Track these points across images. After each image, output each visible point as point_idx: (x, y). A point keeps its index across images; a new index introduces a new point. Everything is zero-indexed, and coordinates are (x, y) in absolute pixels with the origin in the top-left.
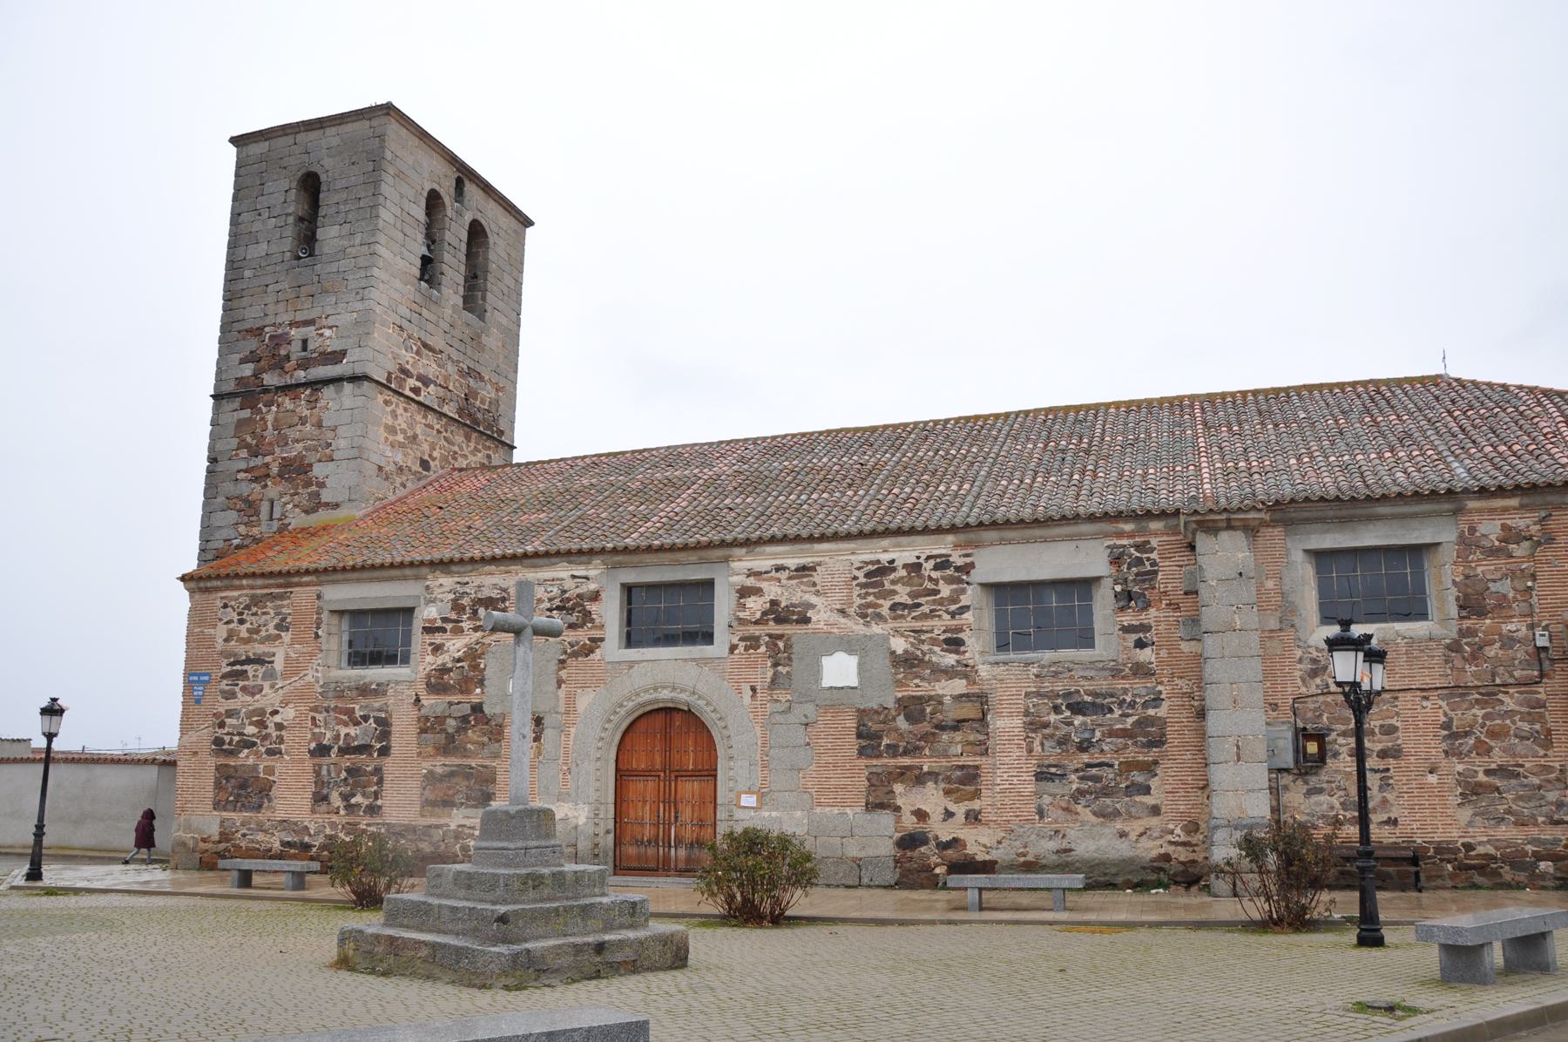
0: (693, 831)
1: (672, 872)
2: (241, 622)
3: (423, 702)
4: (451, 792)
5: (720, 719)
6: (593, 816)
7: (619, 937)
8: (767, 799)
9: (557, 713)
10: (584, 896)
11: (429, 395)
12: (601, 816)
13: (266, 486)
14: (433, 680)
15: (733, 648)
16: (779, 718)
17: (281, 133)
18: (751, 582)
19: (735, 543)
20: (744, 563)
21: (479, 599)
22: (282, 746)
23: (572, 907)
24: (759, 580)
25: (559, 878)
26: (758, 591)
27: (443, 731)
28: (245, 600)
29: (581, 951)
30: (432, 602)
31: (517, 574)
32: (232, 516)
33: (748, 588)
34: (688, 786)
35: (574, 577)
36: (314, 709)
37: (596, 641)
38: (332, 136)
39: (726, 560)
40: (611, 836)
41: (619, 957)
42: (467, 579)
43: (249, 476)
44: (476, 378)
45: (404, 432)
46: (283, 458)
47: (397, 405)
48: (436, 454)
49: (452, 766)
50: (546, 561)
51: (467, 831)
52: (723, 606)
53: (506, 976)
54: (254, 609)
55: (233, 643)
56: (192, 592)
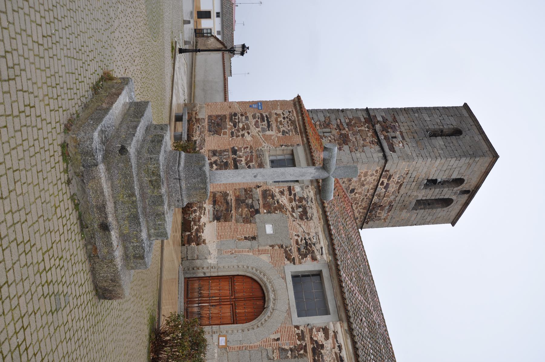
0: (206, 314)
1: (186, 305)
2: (284, 118)
3: (258, 189)
4: (220, 203)
5: (262, 324)
6: (212, 266)
7: (115, 243)
8: (224, 351)
9: (258, 246)
10: (147, 221)
11: (381, 189)
12: (212, 270)
13: (336, 130)
14: (268, 192)
15: (297, 327)
16: (265, 354)
17: (474, 120)
18: (331, 334)
19: (350, 324)
20: (340, 329)
21: (306, 208)
22: (235, 137)
23: (136, 207)
24: (332, 337)
25: (158, 200)
26: (327, 337)
27: (246, 198)
28: (293, 119)
29: (101, 212)
30: (302, 189)
31: (320, 223)
32: (323, 119)
33: (328, 332)
34: (228, 310)
35: (322, 248)
36: (251, 147)
37: (293, 261)
38: (478, 138)
39: (340, 320)
40: (202, 275)
41: (99, 244)
42: (314, 202)
43: (339, 123)
44: (389, 209)
45: (365, 180)
46: (348, 135)
47: (376, 176)
48: (357, 195)
49: (231, 202)
50: (327, 235)
51: (203, 212)
52: (317, 321)
53: (76, 147)
54: (290, 122)
55: (275, 116)
56: (294, 100)
